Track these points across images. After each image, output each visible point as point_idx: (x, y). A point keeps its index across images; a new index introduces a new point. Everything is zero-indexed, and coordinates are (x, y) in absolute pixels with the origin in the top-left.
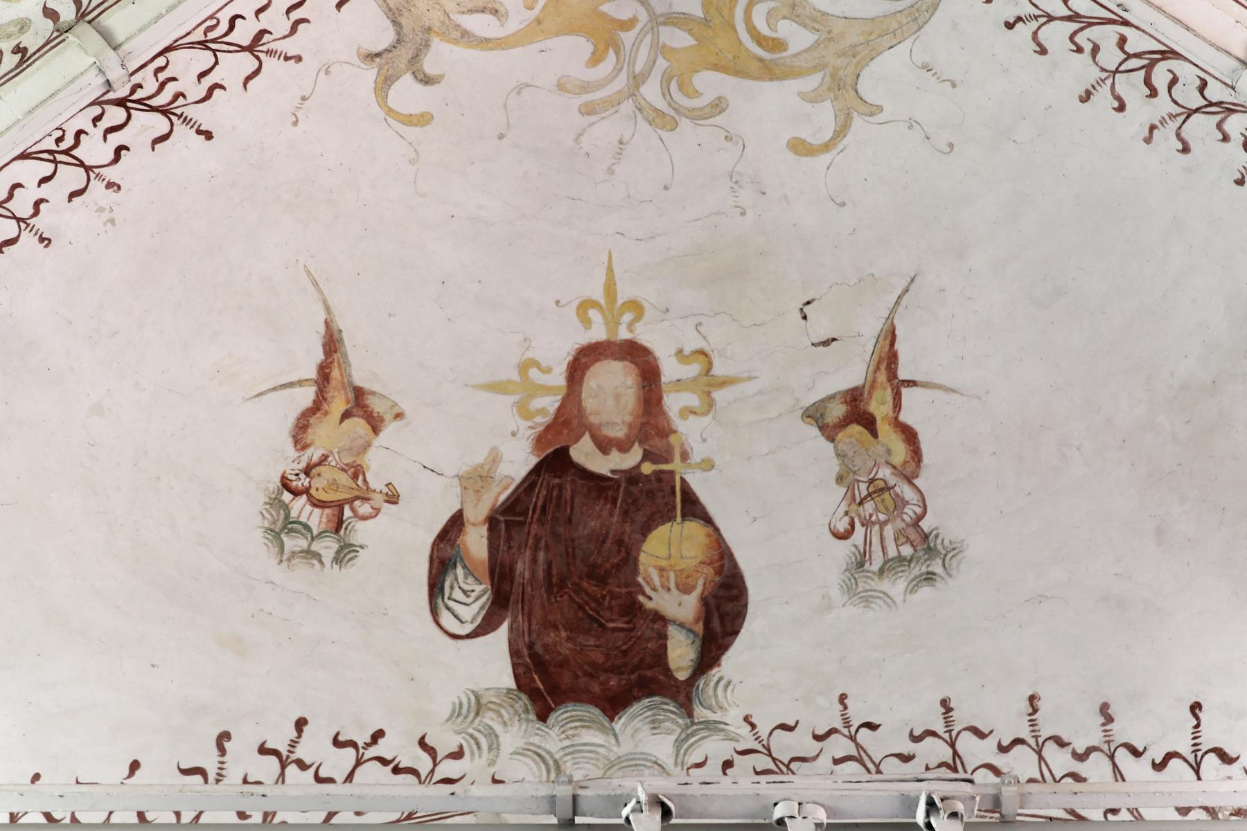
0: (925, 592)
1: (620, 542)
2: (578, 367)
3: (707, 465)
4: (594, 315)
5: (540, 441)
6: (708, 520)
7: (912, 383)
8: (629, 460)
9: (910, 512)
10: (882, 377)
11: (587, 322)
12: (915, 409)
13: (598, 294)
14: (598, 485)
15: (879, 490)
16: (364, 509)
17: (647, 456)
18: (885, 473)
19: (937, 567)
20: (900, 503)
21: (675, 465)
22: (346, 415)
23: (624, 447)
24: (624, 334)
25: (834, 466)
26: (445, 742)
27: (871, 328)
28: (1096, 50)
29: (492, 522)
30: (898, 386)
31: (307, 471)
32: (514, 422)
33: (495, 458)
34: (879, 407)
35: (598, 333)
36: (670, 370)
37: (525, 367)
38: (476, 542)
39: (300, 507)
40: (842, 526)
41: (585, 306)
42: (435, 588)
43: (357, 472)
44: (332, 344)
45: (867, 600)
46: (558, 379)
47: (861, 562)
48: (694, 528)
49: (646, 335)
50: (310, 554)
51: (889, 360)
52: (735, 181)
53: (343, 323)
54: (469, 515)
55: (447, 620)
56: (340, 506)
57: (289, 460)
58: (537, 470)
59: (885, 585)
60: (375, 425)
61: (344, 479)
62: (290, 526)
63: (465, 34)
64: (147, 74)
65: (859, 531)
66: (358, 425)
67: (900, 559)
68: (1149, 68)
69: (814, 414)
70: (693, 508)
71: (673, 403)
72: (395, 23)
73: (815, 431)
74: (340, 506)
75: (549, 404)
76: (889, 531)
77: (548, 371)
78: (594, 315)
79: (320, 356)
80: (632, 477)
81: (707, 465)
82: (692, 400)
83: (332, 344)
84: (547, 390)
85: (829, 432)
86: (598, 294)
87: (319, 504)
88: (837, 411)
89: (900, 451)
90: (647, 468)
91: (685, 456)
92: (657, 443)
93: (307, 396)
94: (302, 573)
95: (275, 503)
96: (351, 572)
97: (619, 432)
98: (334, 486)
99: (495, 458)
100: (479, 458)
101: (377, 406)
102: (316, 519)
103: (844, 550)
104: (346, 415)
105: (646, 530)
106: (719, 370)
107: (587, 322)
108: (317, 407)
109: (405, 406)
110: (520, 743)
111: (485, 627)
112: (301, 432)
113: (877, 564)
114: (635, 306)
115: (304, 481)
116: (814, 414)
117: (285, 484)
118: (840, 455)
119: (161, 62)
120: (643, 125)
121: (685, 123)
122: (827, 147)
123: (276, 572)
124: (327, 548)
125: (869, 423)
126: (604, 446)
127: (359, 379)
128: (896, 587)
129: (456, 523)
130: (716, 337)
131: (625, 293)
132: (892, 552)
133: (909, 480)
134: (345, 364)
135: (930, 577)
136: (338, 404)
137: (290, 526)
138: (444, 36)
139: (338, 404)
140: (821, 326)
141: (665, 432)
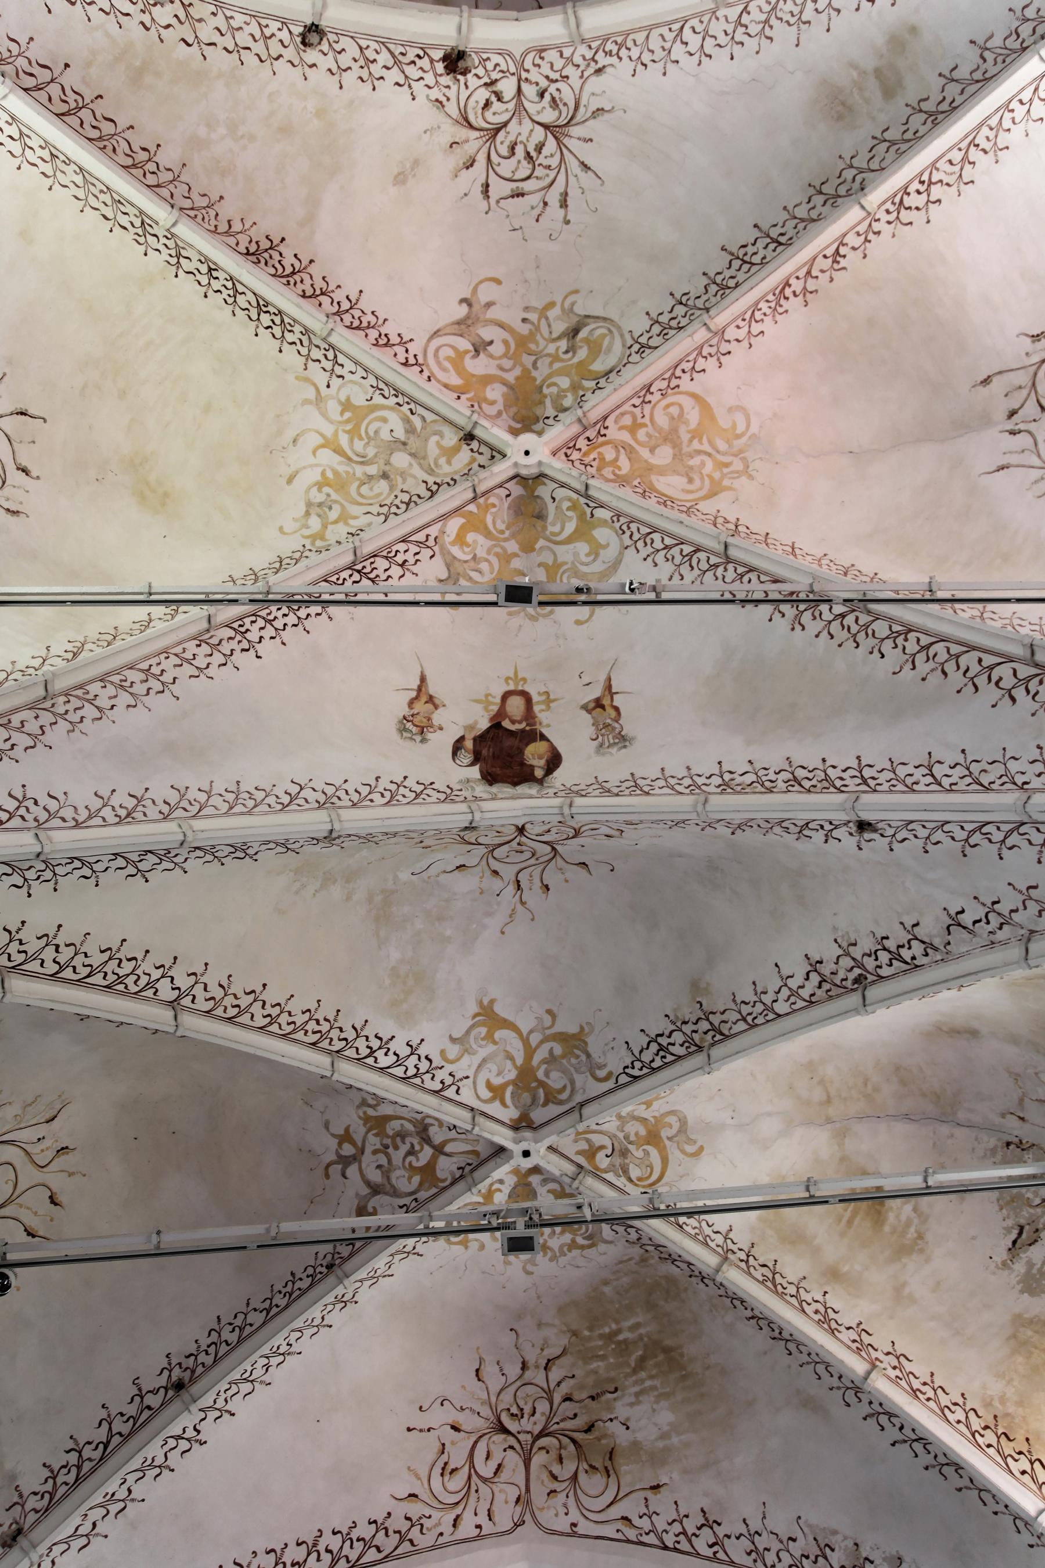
0: (624, 750)
1: (518, 748)
2: (506, 696)
3: (548, 726)
4: (510, 682)
5: (491, 719)
6: (548, 740)
7: (617, 693)
8: (523, 726)
9: (617, 731)
10: (607, 693)
11: (508, 684)
12: (618, 701)
13: (512, 675)
14: (511, 733)
15: (606, 726)
16: (431, 730)
17: (528, 725)
18: (609, 721)
19: (627, 743)
20: (614, 729)
21: (538, 727)
22: (426, 702)
23: (520, 722)
24: (520, 688)
25: (591, 721)
26: (456, 787)
27: (603, 678)
28: (673, 558)
29: (475, 739)
30: (612, 695)
31: (412, 716)
32: (482, 712)
33: (476, 722)
34: (606, 702)
35: (512, 687)
36: (535, 698)
37: (487, 695)
38: (469, 744)
39: (409, 725)
40: (594, 737)
41: (507, 679)
42: (454, 754)
43: (429, 719)
44: (423, 679)
45: (603, 754)
46: (498, 700)
47: (601, 745)
48: (544, 744)
49: (527, 688)
50: (411, 738)
51: (608, 687)
52: (557, 637)
53: (427, 673)
54: (467, 736)
55: (458, 761)
56: (423, 728)
57: (406, 711)
58: (490, 727)
59: (610, 750)
60: (436, 707)
61: (425, 720)
62: (405, 730)
63: (471, 578)
64: (367, 563)
65: (600, 738)
66: (430, 706)
67: (615, 743)
68: (690, 559)
69: (585, 707)
70: (543, 737)
71: (536, 709)
72: (448, 569)
73: (584, 712)
74: (423, 728)
75: (495, 708)
76: (610, 737)
77: (494, 697)
78: (510, 682)
79: (418, 682)
80: (523, 731)
81: (548, 726)
82: (543, 707)
83: (423, 679)
84: (494, 704)
85: (589, 712)
86: (512, 675)
87: (417, 726)
88: (592, 705)
89: (613, 714)
90: (528, 728)
91: (540, 724)
92: (531, 721)
93: (414, 694)
94: (409, 744)
95: (401, 722)
96: (424, 746)
97: (518, 718)
98: (421, 721)
99: (476, 722)
100: (471, 722)
101: (437, 701)
102: (414, 730)
103: (596, 743)
104: (426, 702)
105: (527, 745)
106: (552, 697)
107: (508, 684)
108: (417, 698)
109: (446, 702)
110: (479, 726)
111: (472, 764)
112: (411, 703)
113: (607, 744)
114: (524, 680)
115: (411, 718)
116: (585, 707)
117: (405, 718)
118: (593, 718)
119: (372, 560)
120: (527, 620)
121: (541, 619)
122: (587, 621)
123: (400, 741)
124: (418, 738)
125: (603, 707)
126: (513, 722)
127: (431, 692)
128: (614, 750)
129: (462, 739)
130: (551, 687)
131: (520, 676)
132: (612, 741)
133: (617, 721)
134: (427, 686)
135: (625, 747)
136: (424, 699)
137: (405, 730)
138: (464, 578)
139: (424, 699)
140: (586, 679)
141: (534, 717)
